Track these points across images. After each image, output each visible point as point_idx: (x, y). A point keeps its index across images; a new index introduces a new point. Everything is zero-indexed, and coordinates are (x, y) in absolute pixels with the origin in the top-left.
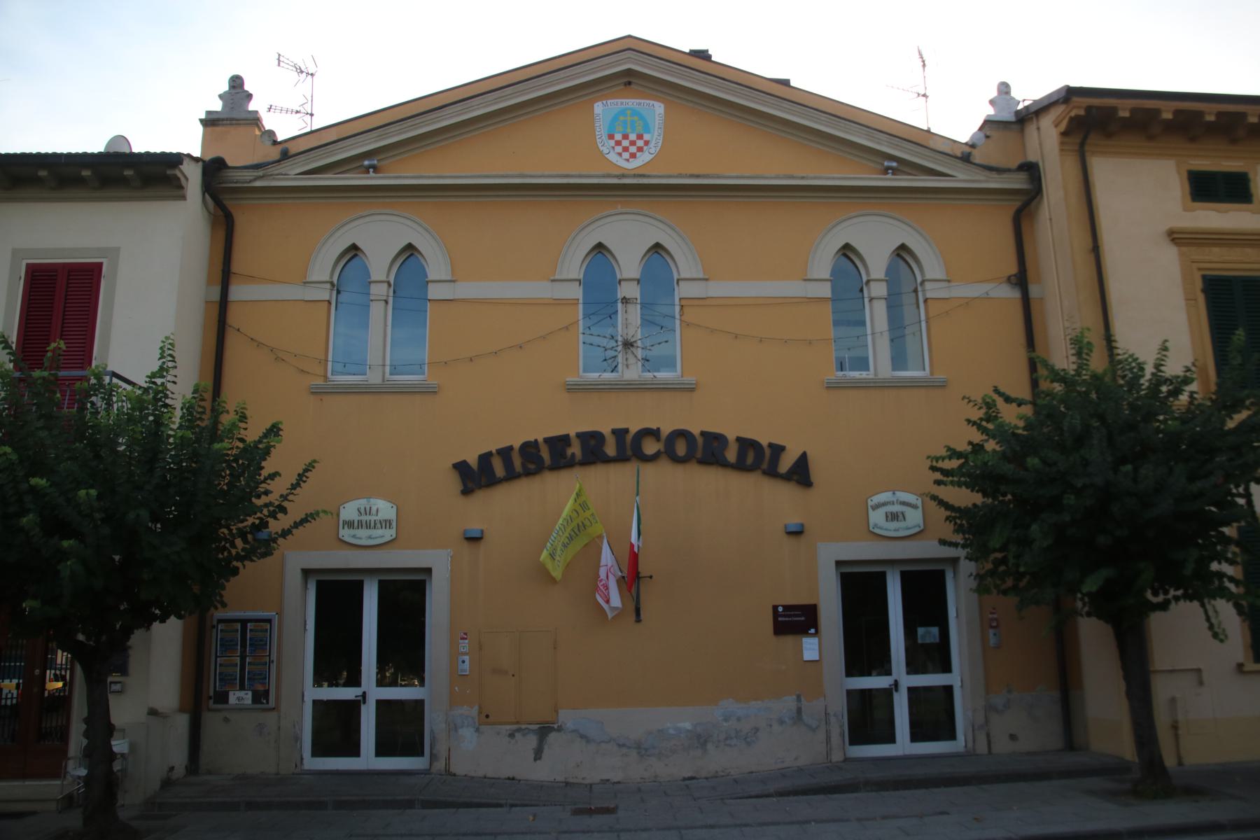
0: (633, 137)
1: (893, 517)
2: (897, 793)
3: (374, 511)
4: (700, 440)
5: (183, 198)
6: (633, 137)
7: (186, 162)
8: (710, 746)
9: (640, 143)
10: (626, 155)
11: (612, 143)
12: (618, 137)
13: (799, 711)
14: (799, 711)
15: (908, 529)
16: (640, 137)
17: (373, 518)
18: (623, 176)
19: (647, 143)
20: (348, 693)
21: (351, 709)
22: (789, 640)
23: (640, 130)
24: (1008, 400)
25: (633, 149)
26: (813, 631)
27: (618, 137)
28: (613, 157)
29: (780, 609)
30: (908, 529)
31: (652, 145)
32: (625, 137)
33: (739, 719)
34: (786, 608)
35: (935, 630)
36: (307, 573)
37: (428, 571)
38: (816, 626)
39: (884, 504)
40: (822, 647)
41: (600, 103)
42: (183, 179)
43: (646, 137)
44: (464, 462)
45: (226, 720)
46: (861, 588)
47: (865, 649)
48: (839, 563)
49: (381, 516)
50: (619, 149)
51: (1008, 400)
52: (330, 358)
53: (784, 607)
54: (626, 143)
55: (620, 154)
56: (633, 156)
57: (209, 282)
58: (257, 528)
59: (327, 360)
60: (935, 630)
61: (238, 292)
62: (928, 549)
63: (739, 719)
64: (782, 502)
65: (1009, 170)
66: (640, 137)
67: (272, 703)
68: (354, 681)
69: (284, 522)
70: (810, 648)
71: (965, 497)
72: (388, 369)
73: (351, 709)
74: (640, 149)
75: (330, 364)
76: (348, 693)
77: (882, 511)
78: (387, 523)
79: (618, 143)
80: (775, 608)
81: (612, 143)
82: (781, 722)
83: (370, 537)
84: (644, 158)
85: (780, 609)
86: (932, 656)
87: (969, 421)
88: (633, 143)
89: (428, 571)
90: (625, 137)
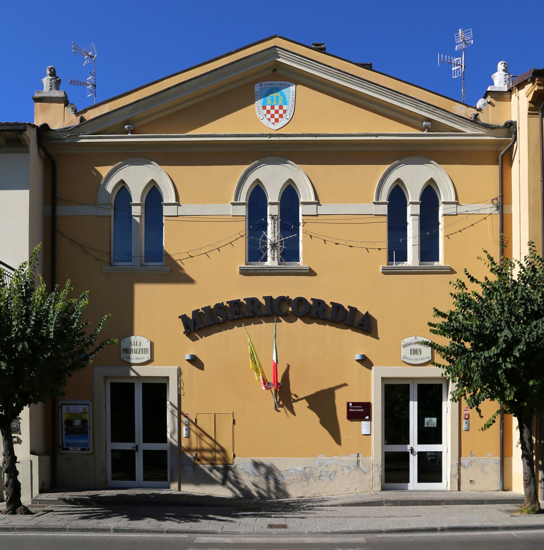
0: (277, 107)
1: (415, 352)
2: (401, 507)
3: (138, 343)
4: (263, 302)
5: (28, 152)
6: (277, 107)
7: (28, 128)
8: (311, 479)
9: (281, 112)
10: (273, 120)
11: (265, 112)
12: (268, 108)
13: (358, 462)
14: (358, 462)
15: (422, 359)
16: (281, 107)
17: (138, 347)
18: (271, 135)
19: (285, 112)
20: (127, 446)
21: (130, 455)
22: (355, 423)
23: (281, 103)
24: (473, 280)
25: (277, 116)
26: (367, 417)
27: (268, 108)
28: (265, 122)
29: (351, 404)
30: (422, 359)
31: (288, 113)
32: (272, 107)
33: (327, 466)
34: (354, 404)
35: (434, 420)
36: (106, 378)
37: (167, 378)
38: (370, 414)
39: (410, 344)
40: (373, 428)
41: (258, 84)
42: (27, 141)
43: (285, 107)
44: (185, 315)
45: (69, 459)
46: (395, 394)
47: (395, 430)
48: (383, 379)
49: (143, 347)
50: (269, 116)
51: (473, 280)
52: (112, 252)
53: (352, 403)
54: (273, 112)
55: (269, 119)
56: (277, 120)
57: (45, 204)
58: (81, 351)
59: (110, 253)
60: (434, 420)
61: (62, 210)
62: (434, 373)
63: (327, 466)
64: (355, 342)
65: (498, 127)
66: (281, 107)
67: (91, 451)
68: (132, 439)
69: (92, 348)
70: (364, 426)
71: (445, 341)
72: (143, 258)
73: (130, 455)
74: (281, 116)
75: (112, 255)
76: (127, 446)
77: (408, 348)
78: (144, 351)
79: (268, 112)
80: (348, 403)
81: (265, 112)
82: (349, 468)
83: (137, 359)
84: (283, 122)
85: (351, 404)
86: (432, 435)
87: (451, 294)
88: (277, 112)
89: (167, 378)
90: (272, 107)
